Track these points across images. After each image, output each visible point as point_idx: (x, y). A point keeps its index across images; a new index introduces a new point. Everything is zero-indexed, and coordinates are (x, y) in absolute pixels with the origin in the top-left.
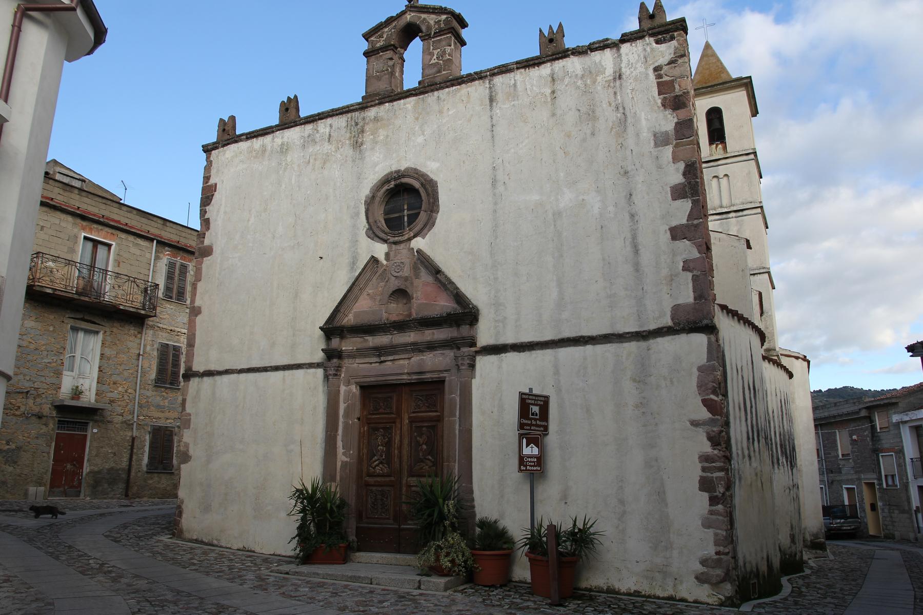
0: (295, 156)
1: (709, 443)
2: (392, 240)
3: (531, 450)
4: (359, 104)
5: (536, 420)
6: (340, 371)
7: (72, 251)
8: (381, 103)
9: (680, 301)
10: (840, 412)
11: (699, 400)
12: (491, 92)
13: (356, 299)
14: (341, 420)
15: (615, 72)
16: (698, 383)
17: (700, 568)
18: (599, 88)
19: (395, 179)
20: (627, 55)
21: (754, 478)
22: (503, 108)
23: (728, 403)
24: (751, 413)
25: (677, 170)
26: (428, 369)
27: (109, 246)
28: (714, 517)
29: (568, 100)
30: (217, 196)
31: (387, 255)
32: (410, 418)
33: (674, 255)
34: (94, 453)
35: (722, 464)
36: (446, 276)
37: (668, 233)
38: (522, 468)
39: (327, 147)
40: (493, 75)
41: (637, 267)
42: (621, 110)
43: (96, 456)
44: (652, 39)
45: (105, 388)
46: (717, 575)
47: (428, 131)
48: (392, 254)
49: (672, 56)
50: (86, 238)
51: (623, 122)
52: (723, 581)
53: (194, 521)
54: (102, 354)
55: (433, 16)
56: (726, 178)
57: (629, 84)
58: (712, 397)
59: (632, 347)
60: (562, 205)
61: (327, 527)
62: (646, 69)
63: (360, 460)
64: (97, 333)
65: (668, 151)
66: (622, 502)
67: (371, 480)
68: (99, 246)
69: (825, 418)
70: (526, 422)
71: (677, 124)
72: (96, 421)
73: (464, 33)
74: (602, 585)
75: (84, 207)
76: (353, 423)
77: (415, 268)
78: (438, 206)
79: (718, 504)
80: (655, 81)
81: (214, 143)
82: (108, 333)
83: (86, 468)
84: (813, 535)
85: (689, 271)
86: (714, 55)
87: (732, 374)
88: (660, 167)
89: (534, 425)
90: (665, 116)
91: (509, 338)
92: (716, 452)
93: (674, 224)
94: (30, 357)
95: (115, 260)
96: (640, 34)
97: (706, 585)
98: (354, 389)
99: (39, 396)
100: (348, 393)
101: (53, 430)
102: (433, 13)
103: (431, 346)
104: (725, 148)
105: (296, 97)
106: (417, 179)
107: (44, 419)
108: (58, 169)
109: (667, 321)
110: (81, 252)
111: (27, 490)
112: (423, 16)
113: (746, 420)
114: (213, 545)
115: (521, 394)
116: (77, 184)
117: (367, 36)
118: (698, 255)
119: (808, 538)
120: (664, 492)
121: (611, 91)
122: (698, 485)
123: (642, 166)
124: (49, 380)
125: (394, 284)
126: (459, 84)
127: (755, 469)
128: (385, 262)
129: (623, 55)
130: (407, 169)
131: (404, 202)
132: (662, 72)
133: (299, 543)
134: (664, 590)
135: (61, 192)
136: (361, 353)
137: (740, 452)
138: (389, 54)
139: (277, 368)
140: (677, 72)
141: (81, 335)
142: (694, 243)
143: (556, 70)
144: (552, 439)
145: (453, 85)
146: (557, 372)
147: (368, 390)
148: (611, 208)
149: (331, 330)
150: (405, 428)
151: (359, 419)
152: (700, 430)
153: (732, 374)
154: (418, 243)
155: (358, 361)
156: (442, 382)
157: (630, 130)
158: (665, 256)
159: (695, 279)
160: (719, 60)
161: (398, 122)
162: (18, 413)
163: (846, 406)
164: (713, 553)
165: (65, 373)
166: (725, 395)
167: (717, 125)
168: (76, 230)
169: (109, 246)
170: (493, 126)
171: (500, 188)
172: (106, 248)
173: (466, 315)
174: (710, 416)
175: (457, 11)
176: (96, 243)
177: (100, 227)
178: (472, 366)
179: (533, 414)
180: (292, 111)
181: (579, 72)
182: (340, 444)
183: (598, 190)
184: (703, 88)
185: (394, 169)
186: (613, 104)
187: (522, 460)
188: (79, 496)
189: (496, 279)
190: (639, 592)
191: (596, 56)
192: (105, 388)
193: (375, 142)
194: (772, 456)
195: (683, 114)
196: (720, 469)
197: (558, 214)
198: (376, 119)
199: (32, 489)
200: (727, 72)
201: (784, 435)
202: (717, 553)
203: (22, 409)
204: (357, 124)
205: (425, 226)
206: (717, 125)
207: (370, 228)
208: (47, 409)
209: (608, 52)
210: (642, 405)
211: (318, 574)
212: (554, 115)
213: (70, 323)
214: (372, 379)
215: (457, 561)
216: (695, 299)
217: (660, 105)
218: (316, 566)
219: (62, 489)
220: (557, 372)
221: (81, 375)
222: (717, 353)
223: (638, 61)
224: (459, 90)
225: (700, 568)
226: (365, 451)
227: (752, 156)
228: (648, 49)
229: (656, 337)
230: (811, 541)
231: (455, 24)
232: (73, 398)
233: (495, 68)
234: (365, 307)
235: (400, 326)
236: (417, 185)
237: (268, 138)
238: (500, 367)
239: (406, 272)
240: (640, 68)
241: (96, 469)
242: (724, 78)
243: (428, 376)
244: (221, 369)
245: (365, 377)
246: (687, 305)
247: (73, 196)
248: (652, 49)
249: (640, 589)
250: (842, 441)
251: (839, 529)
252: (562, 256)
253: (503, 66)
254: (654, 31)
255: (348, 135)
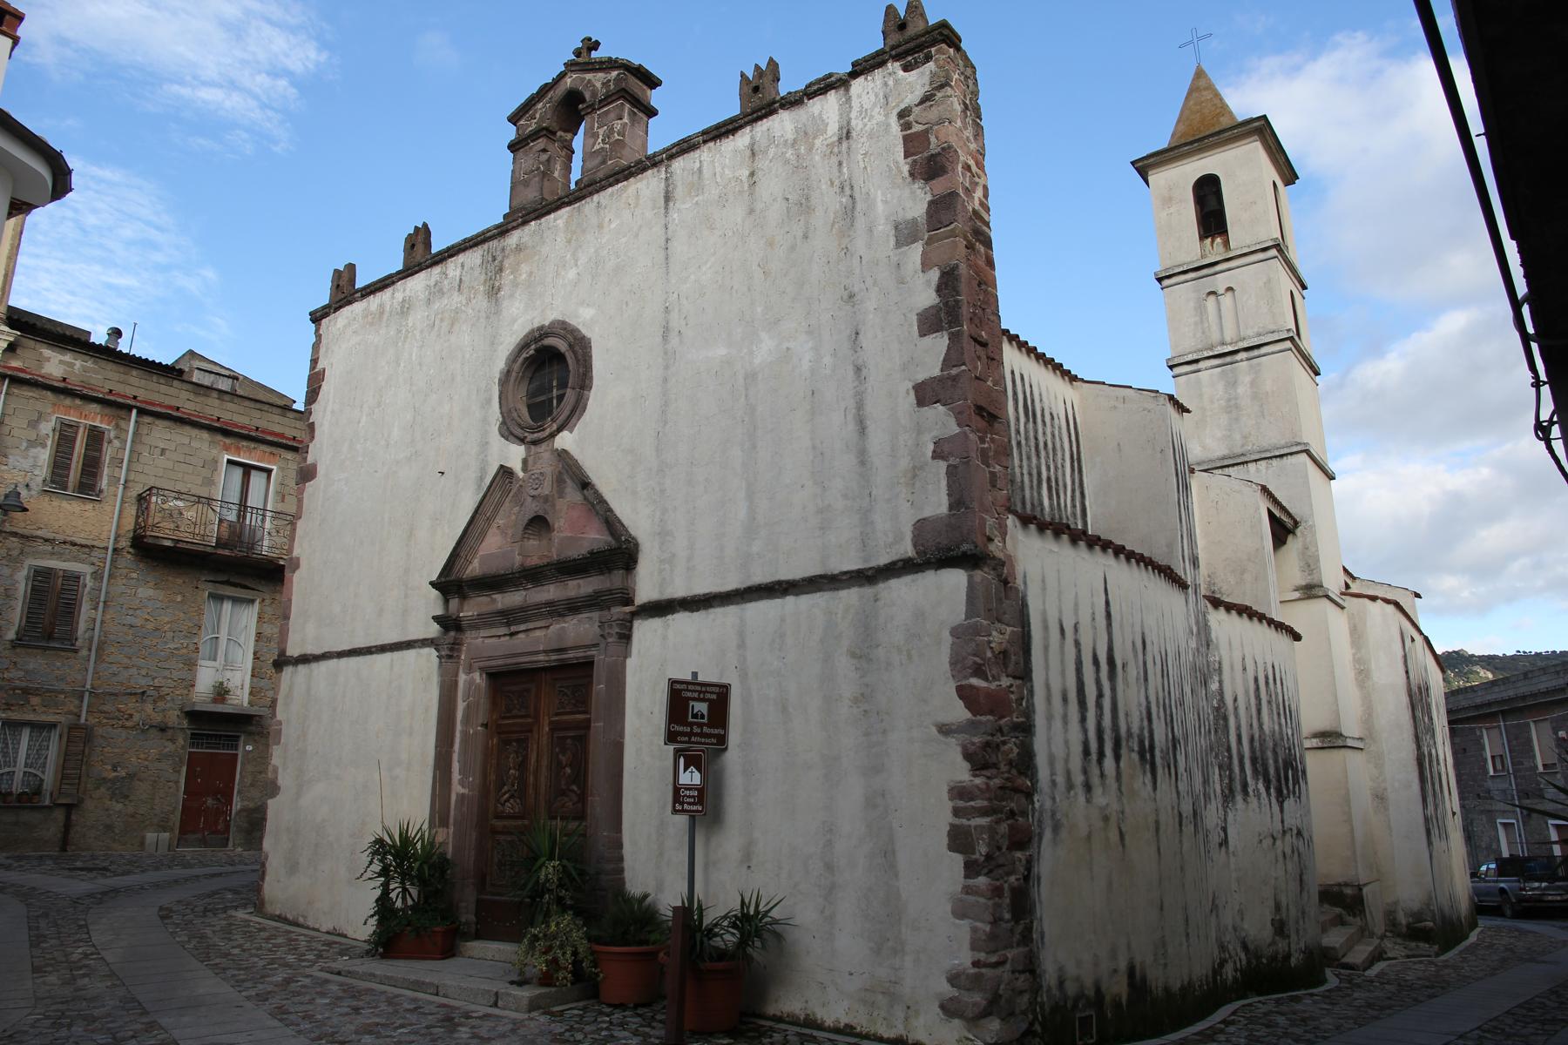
0: (417, 317)
1: (966, 765)
2: (530, 437)
3: (691, 777)
4: (497, 227)
5: (701, 725)
6: (459, 651)
7: (210, 482)
8: (525, 223)
9: (928, 512)
10: (1534, 689)
11: (951, 688)
12: (667, 186)
13: (483, 535)
14: (459, 727)
15: (841, 128)
16: (951, 657)
17: (947, 990)
18: (817, 158)
19: (536, 340)
20: (859, 96)
21: (1100, 824)
22: (684, 207)
23: (1031, 692)
24: (1099, 706)
25: (928, 282)
26: (569, 644)
27: (269, 472)
28: (971, 898)
29: (773, 185)
30: (325, 386)
31: (525, 462)
32: (551, 723)
33: (919, 432)
34: (248, 781)
35: (985, 803)
36: (596, 492)
37: (912, 393)
38: (678, 807)
39: (456, 299)
40: (671, 157)
41: (863, 458)
42: (848, 192)
43: (252, 785)
44: (897, 64)
45: (262, 683)
46: (975, 1004)
47: (583, 259)
48: (530, 460)
49: (927, 88)
50: (229, 461)
51: (849, 212)
52: (986, 1013)
53: (279, 888)
54: (259, 635)
55: (601, 75)
56: (1229, 294)
57: (860, 145)
58: (975, 681)
59: (851, 596)
60: (757, 361)
61: (427, 899)
62: (886, 116)
63: (484, 791)
64: (252, 601)
65: (916, 250)
66: (829, 867)
67: (499, 824)
68: (253, 473)
69: (1511, 700)
70: (681, 729)
71: (931, 203)
72: (251, 734)
73: (655, 98)
74: (797, 1012)
75: (226, 416)
76: (476, 733)
77: (559, 481)
78: (591, 378)
79: (978, 874)
80: (900, 135)
81: (324, 308)
82: (267, 602)
83: (237, 804)
84: (1413, 914)
85: (943, 458)
86: (1210, 87)
87: (1046, 638)
88: (901, 281)
89: (696, 735)
90: (913, 193)
91: (679, 591)
92: (978, 781)
93: (920, 377)
94: (147, 642)
95: (277, 493)
96: (878, 59)
97: (957, 1022)
98: (477, 677)
99: (162, 698)
100: (470, 683)
101: (183, 747)
102: (600, 70)
103: (573, 607)
104: (1226, 243)
105: (425, 225)
106: (563, 338)
107: (170, 732)
108: (197, 364)
109: (907, 549)
110: (227, 485)
111: (144, 838)
112: (588, 76)
113: (1083, 719)
114: (298, 925)
115: (672, 682)
116: (224, 385)
117: (514, 119)
118: (957, 430)
119: (1403, 920)
120: (894, 852)
121: (834, 160)
122: (945, 841)
123: (875, 284)
124: (176, 675)
125: (532, 508)
126: (626, 179)
127: (1102, 809)
128: (521, 474)
129: (854, 99)
130: (553, 323)
131: (549, 374)
132: (911, 118)
133: (380, 923)
134: (891, 1026)
135: (192, 397)
136: (484, 621)
137: (1060, 779)
138: (541, 143)
139: (383, 649)
140: (933, 114)
141: (227, 606)
142: (951, 410)
143: (758, 136)
144: (733, 757)
145: (618, 182)
146: (742, 645)
147: (497, 677)
148: (827, 360)
149: (450, 584)
150: (545, 740)
151: (485, 725)
152: (952, 741)
153: (1046, 638)
154: (565, 440)
155: (484, 633)
156: (587, 665)
157: (861, 222)
158: (908, 434)
159: (951, 472)
160: (1217, 95)
161: (545, 249)
162: (128, 724)
163: (1544, 678)
164: (968, 963)
165: (201, 662)
166: (1025, 675)
167: (1212, 205)
168: (214, 452)
169: (269, 472)
170: (667, 240)
171: (674, 341)
172: (265, 475)
173: (620, 554)
174: (969, 715)
175: (636, 62)
176: (247, 469)
177: (253, 445)
178: (626, 637)
179: (695, 716)
180: (420, 248)
181: (790, 136)
182: (456, 766)
183: (810, 332)
184: (1186, 144)
185: (536, 325)
186: (837, 183)
187: (677, 790)
188: (226, 845)
189: (662, 491)
190: (852, 1027)
191: (815, 106)
192: (262, 683)
193: (515, 285)
194: (1231, 779)
195: (940, 185)
196: (984, 812)
197: (751, 377)
198: (519, 249)
199: (151, 837)
200: (1230, 113)
201: (1262, 741)
202: (976, 964)
203: (136, 717)
204: (494, 259)
205: (573, 412)
206: (1212, 205)
207: (504, 423)
208: (174, 718)
209: (832, 95)
210: (863, 697)
211: (374, 975)
212: (751, 211)
213: (210, 588)
214: (500, 662)
215: (562, 961)
216: (951, 507)
217: (906, 174)
218: (401, 963)
219: (199, 836)
220: (742, 645)
221: (229, 665)
222: (1001, 598)
223: (875, 105)
224: (625, 189)
225: (947, 990)
226: (493, 777)
227: (1274, 252)
228: (891, 83)
229: (888, 579)
230: (1408, 926)
231: (635, 85)
232: (215, 701)
233: (674, 145)
234: (496, 550)
235: (532, 576)
236: (562, 346)
237: (388, 292)
238: (665, 638)
239: (546, 489)
240: (878, 116)
241: (252, 805)
242: (1225, 122)
243: (571, 655)
244: (318, 652)
245: (490, 658)
246: (936, 520)
247: (210, 401)
248: (896, 81)
249: (854, 1022)
250: (1491, 743)
251: (1539, 899)
252: (754, 447)
253: (684, 141)
254: (899, 50)
255: (483, 277)
